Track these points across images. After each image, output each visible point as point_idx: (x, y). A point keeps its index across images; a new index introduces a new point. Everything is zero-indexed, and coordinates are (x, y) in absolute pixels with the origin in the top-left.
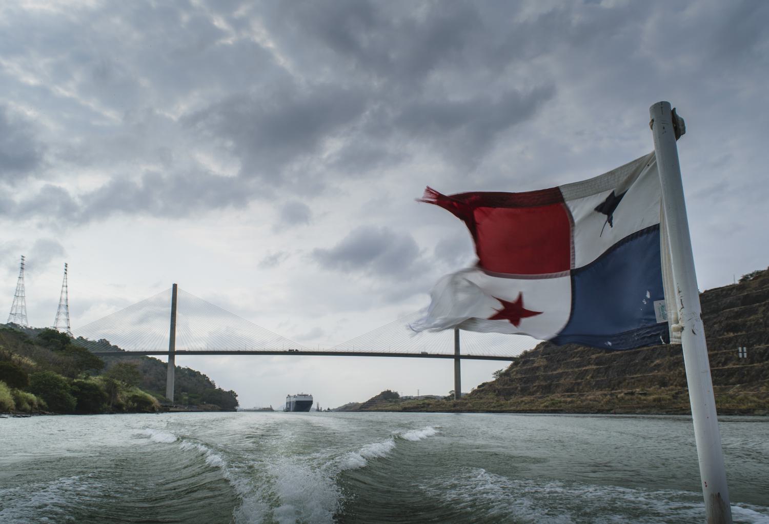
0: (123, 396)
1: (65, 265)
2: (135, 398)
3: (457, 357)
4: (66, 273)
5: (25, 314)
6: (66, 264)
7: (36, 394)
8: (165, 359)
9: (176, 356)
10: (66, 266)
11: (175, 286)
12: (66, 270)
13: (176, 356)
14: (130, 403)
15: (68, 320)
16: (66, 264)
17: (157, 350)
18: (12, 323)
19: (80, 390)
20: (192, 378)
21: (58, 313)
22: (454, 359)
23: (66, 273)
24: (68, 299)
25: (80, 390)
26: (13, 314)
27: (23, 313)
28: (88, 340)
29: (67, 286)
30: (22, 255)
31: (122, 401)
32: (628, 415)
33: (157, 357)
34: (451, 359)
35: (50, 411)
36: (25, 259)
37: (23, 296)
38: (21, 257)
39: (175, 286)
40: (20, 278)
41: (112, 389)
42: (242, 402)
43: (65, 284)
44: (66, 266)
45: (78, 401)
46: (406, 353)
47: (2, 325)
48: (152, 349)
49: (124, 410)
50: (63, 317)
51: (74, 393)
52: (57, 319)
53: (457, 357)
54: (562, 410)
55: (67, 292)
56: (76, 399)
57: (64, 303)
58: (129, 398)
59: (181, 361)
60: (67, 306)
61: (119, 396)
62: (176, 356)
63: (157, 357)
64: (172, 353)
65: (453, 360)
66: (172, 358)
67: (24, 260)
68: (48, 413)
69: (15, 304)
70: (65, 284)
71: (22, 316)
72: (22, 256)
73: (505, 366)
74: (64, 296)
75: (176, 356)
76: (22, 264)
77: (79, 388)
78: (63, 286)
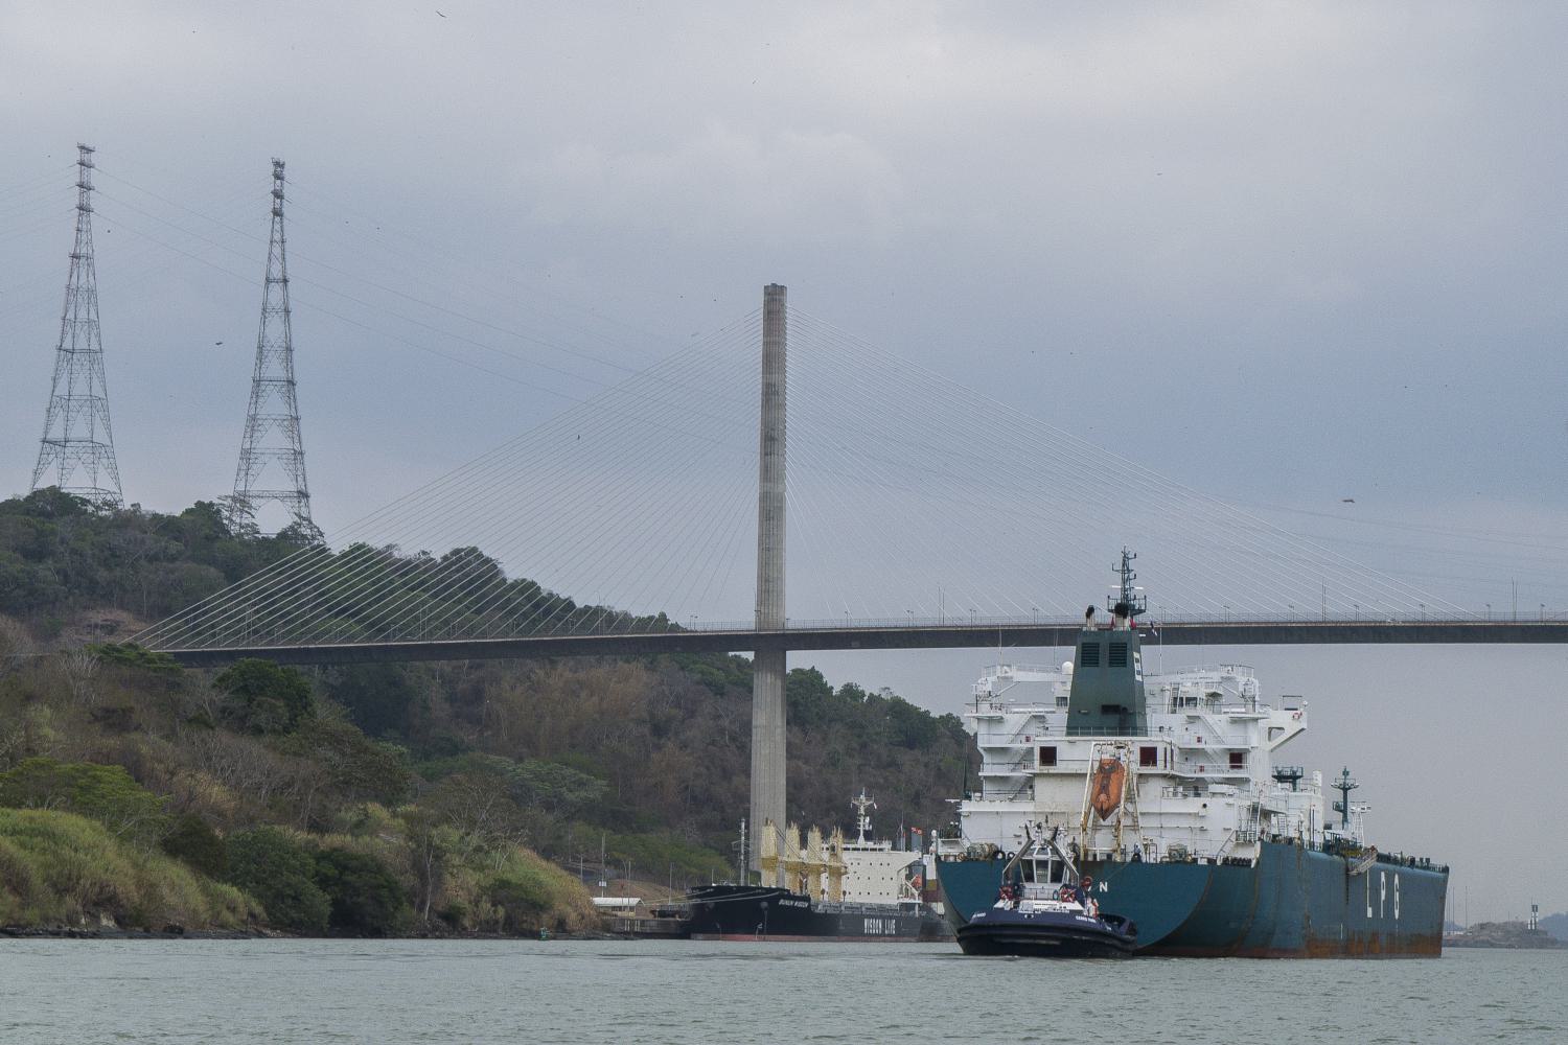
0: (461, 885)
2: (501, 891)
6: (279, 165)
7: (242, 886)
10: (278, 177)
11: (774, 296)
12: (278, 195)
14: (486, 906)
15: (299, 454)
16: (279, 165)
18: (54, 490)
19: (337, 872)
20: (906, 757)
21: (253, 423)
23: (277, 213)
24: (291, 306)
25: (337, 872)
26: (54, 443)
28: (396, 554)
29: (285, 281)
30: (82, 143)
31: (462, 900)
32: (1050, 934)
35: (274, 929)
36: (94, 158)
37: (95, 346)
38: (77, 155)
39: (774, 296)
40: (75, 256)
41: (428, 862)
43: (276, 273)
44: (278, 177)
45: (335, 903)
47: (12, 505)
49: (465, 929)
50: (273, 438)
51: (324, 882)
52: (247, 455)
55: (287, 312)
56: (328, 897)
57: (275, 369)
58: (481, 887)
60: (291, 383)
61: (450, 882)
65: (1072, 650)
68: (268, 932)
69: (62, 390)
70: (276, 273)
71: (95, 447)
72: (82, 148)
74: (275, 330)
77: (336, 868)
78: (268, 281)
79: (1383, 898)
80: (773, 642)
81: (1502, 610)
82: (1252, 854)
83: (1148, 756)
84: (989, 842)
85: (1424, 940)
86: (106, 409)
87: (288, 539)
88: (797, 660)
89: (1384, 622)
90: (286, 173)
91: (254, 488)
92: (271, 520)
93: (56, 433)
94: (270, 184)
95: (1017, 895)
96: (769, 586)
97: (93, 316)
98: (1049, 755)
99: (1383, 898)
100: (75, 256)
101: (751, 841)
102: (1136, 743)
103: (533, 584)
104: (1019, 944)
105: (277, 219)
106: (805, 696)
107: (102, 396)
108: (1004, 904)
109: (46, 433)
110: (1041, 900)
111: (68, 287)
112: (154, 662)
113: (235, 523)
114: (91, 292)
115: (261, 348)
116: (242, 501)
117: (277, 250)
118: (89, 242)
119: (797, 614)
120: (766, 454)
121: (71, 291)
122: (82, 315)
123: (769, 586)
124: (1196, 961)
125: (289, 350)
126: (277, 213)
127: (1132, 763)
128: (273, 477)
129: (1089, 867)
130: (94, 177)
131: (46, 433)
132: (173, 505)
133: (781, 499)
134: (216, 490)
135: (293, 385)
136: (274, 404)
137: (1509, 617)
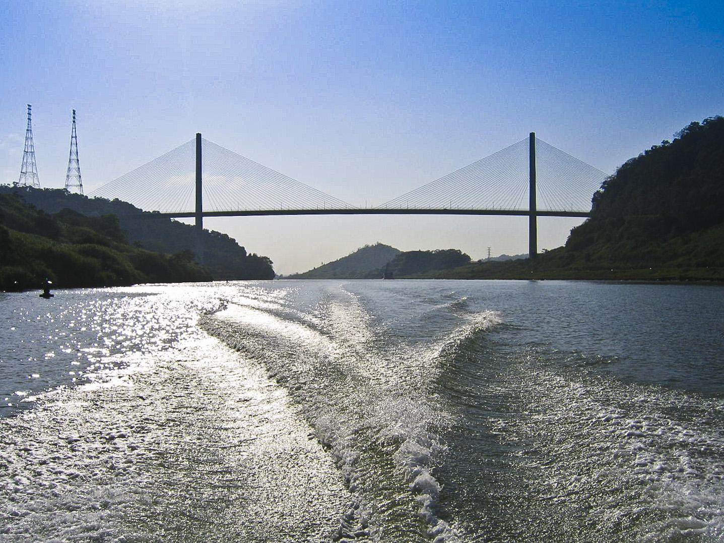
1: (72, 112)
3: (533, 213)
4: (74, 122)
5: (36, 172)
6: (74, 111)
8: (191, 221)
9: (194, 211)
10: (74, 113)
11: (199, 136)
13: (194, 211)
15: (80, 176)
17: (503, 209)
23: (74, 122)
27: (35, 171)
29: (76, 137)
33: (181, 220)
34: (205, 211)
37: (33, 151)
39: (199, 136)
46: (485, 209)
48: (173, 211)
53: (533, 213)
54: (670, 279)
59: (209, 224)
62: (194, 211)
63: (181, 220)
64: (199, 214)
66: (199, 222)
67: (30, 109)
69: (25, 161)
72: (29, 105)
73: (580, 221)
75: (194, 211)
76: (29, 114)
86: (37, 176)
91: (70, 184)
93: (24, 171)
97: (33, 161)
100: (27, 130)
101: (255, 310)
107: (36, 172)
109: (22, 170)
111: (26, 137)
117: (74, 130)
118: (31, 127)
122: (30, 144)
124: (190, 212)
128: (74, 181)
131: (22, 170)
135: (31, 120)
136: (74, 165)
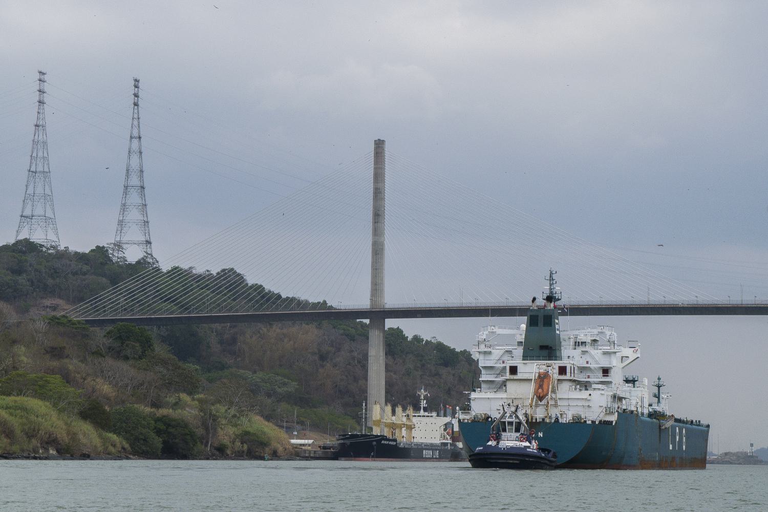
0: (226, 434)
2: (245, 437)
6: (136, 81)
7: (118, 434)
10: (136, 87)
11: (379, 145)
12: (136, 95)
14: (238, 444)
15: (146, 223)
16: (136, 81)
18: (26, 240)
19: (165, 427)
21: (124, 207)
22: (369, 320)
23: (136, 104)
24: (143, 150)
25: (165, 427)
26: (27, 217)
28: (194, 272)
29: (140, 138)
30: (40, 70)
31: (226, 441)
32: (514, 458)
35: (134, 455)
36: (46, 77)
37: (46, 170)
38: (38, 76)
39: (379, 145)
40: (37, 126)
41: (210, 422)
42: (716, 446)
43: (135, 134)
44: (136, 87)
45: (164, 442)
47: (6, 247)
49: (228, 455)
50: (134, 215)
51: (158, 432)
52: (121, 223)
55: (141, 153)
56: (161, 440)
57: (134, 181)
58: (235, 435)
60: (143, 187)
61: (220, 432)
65: (525, 319)
68: (131, 456)
69: (30, 191)
70: (135, 134)
71: (46, 219)
72: (40, 72)
74: (135, 162)
77: (165, 426)
78: (131, 138)
79: (677, 440)
80: (379, 315)
81: (736, 299)
82: (613, 418)
83: (562, 370)
84: (485, 413)
85: (698, 460)
86: (52, 201)
87: (141, 264)
88: (390, 323)
89: (678, 305)
90: (140, 85)
91: (124, 239)
92: (133, 255)
93: (28, 212)
94: (132, 90)
95: (498, 438)
96: (377, 287)
97: (46, 155)
98: (514, 370)
99: (677, 440)
100: (37, 126)
101: (368, 412)
102: (556, 364)
103: (261, 286)
104: (499, 463)
105: (136, 107)
106: (394, 341)
107: (50, 194)
108: (492, 443)
109: (23, 212)
110: (510, 441)
111: (33, 141)
112: (75, 324)
113: (115, 256)
114: (45, 143)
115: (128, 170)
116: (119, 246)
117: (136, 122)
118: (44, 119)
119: (391, 301)
120: (375, 223)
121: (35, 143)
122: (40, 154)
123: (377, 287)
124: (586, 471)
125: (142, 171)
126: (136, 104)
127: (554, 374)
128: (134, 234)
129: (534, 425)
130: (46, 87)
131: (23, 212)
132: (85, 247)
133: (382, 244)
134: (106, 240)
135: (144, 188)
136: (134, 198)
137: (739, 302)
